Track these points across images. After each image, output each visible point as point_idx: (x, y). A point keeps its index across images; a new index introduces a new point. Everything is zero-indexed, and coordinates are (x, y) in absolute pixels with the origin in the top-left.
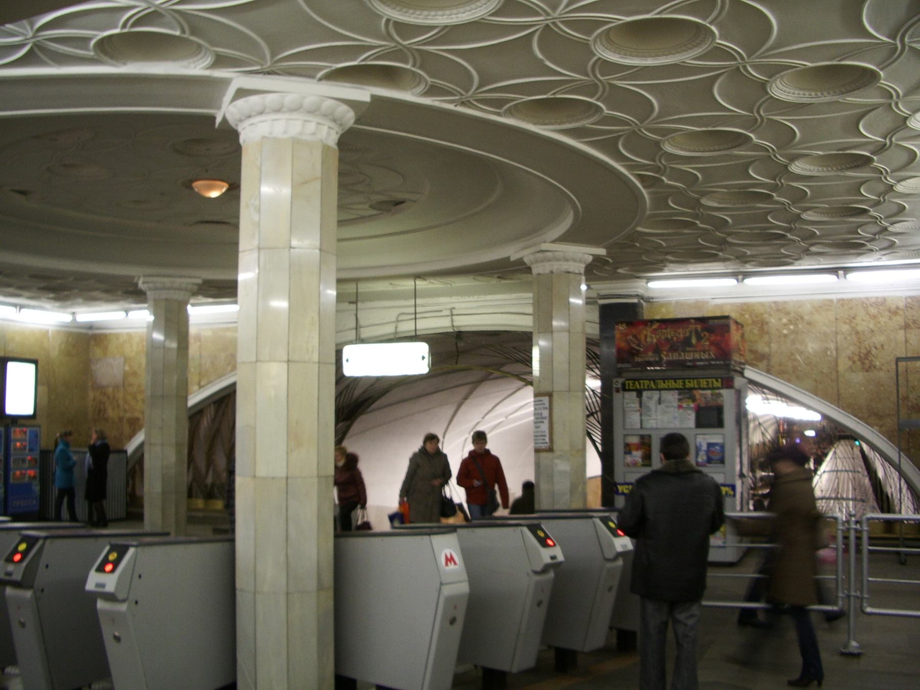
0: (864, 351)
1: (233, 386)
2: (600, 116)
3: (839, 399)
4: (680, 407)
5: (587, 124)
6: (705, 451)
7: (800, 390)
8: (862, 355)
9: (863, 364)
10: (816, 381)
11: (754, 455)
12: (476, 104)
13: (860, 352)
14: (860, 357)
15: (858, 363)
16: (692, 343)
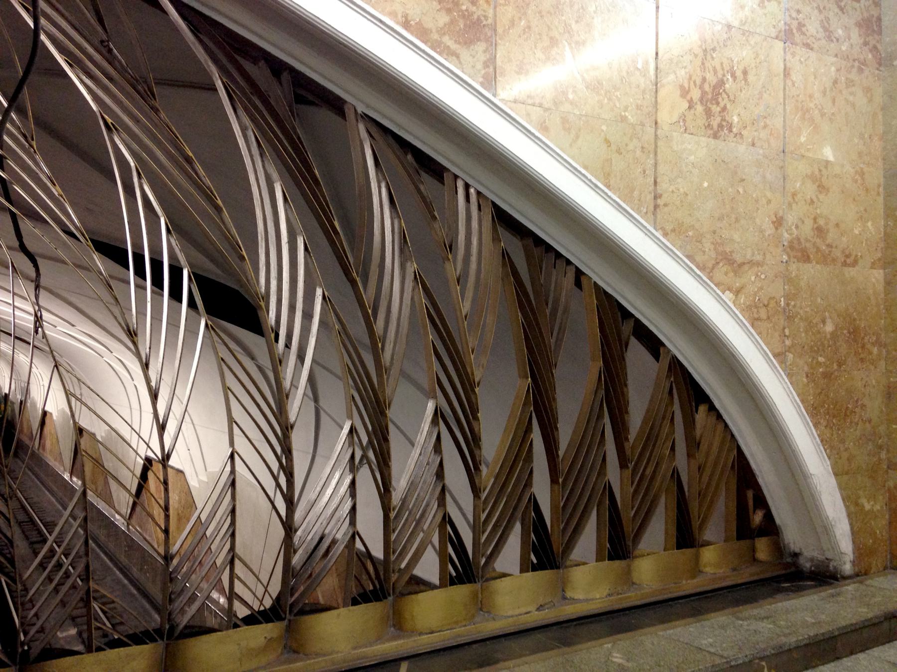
0: (711, 78)
1: (443, 184)
2: (7, 417)
3: (656, 207)
4: (403, 17)
5: (72, 611)
6: (708, 544)
7: (285, 141)
8: (707, 87)
9: (708, 113)
10: (607, 142)
11: (146, 493)
12: (296, 595)
13: (704, 80)
14: (704, 93)
15: (700, 108)
16: (635, 320)
